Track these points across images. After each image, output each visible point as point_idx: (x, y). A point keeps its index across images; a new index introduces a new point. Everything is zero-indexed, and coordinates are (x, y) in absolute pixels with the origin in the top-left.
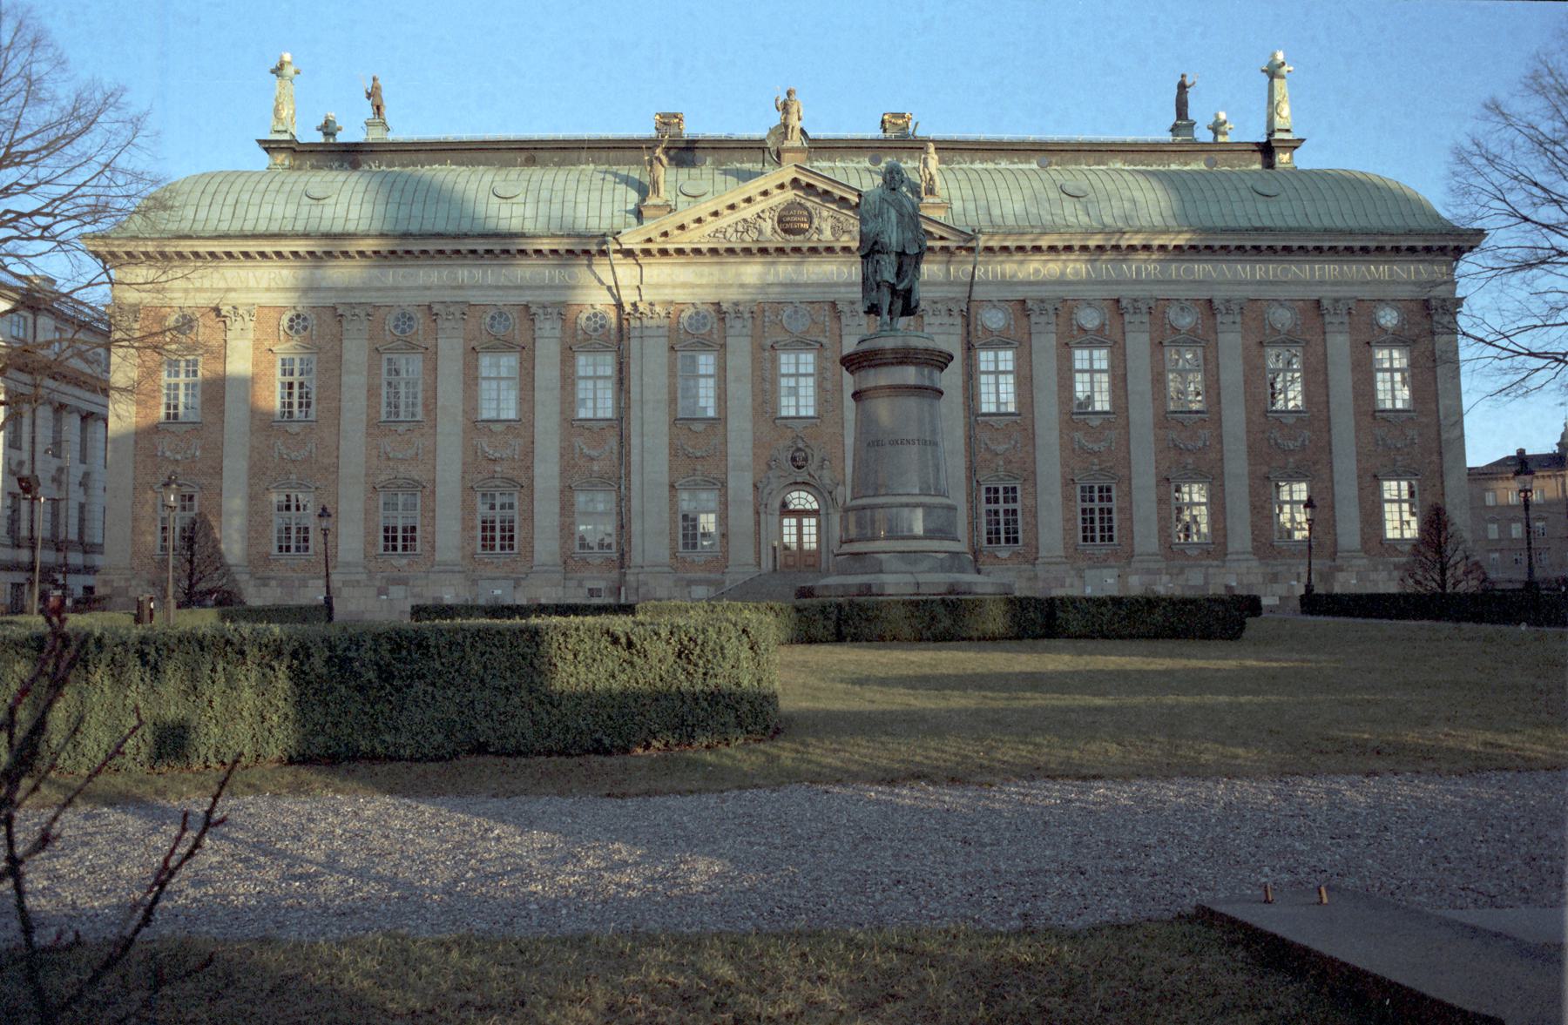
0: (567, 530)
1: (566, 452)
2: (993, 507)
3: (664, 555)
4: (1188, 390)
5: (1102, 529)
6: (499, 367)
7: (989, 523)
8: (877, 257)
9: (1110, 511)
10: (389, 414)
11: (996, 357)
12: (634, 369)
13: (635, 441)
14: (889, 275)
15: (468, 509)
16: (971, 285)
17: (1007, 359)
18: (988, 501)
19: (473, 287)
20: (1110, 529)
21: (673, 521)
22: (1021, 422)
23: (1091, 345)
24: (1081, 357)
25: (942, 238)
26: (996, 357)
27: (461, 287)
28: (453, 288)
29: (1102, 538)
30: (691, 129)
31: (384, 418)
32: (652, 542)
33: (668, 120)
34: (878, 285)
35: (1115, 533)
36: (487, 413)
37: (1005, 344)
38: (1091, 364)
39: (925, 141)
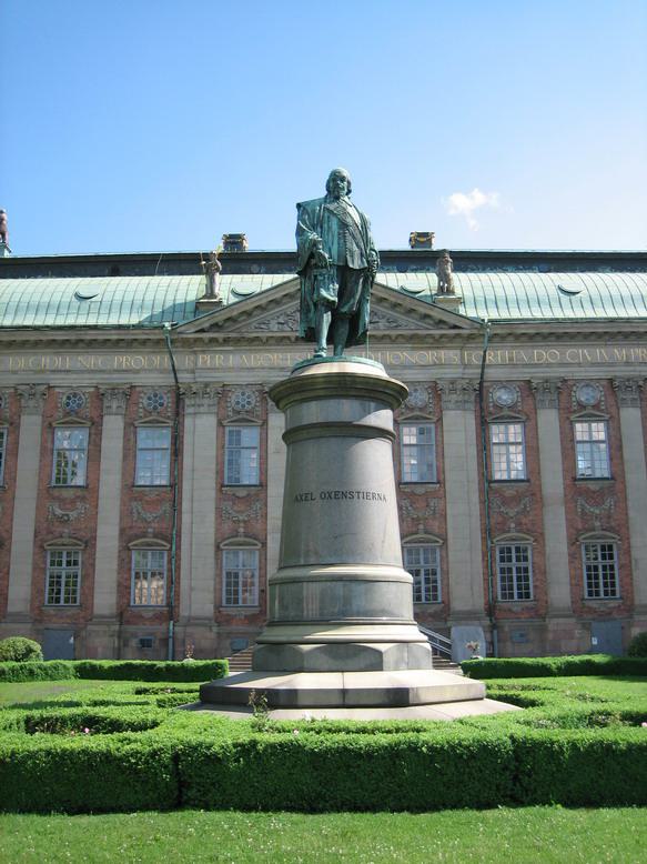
0: (124, 590)
1: (126, 513)
2: (506, 565)
3: (209, 610)
4: (510, 463)
5: (605, 585)
6: (70, 440)
7: (503, 579)
8: (315, 272)
9: (612, 568)
10: (58, 480)
11: (519, 444)
12: (187, 439)
13: (185, 506)
14: (330, 293)
15: (38, 569)
16: (483, 367)
17: (515, 431)
18: (502, 560)
19: (53, 371)
20: (613, 585)
21: (218, 575)
22: (529, 487)
23: (589, 418)
24: (580, 430)
25: (455, 327)
26: (519, 444)
27: (42, 372)
28: (36, 372)
29: (606, 593)
30: (251, 245)
31: (54, 484)
32: (199, 598)
33: (234, 241)
34: (315, 305)
35: (617, 588)
36: (143, 478)
37: (512, 420)
38: (591, 435)
39: (441, 253)
